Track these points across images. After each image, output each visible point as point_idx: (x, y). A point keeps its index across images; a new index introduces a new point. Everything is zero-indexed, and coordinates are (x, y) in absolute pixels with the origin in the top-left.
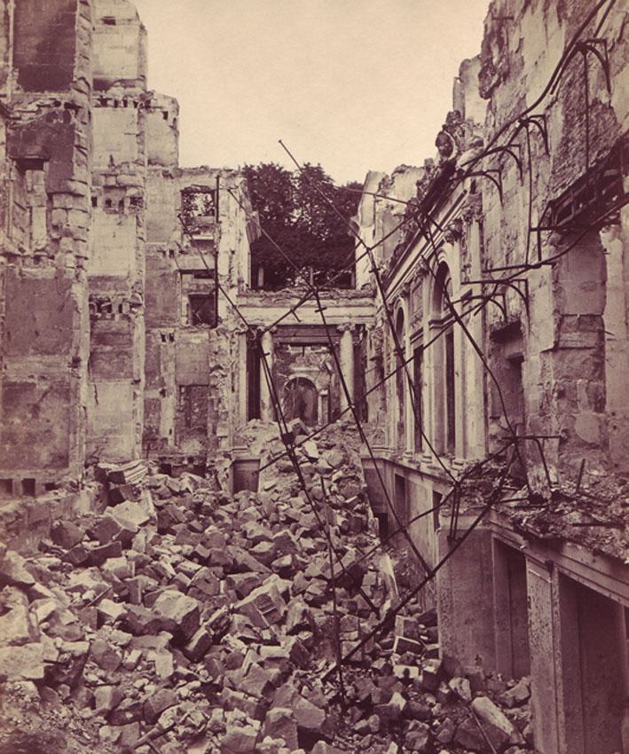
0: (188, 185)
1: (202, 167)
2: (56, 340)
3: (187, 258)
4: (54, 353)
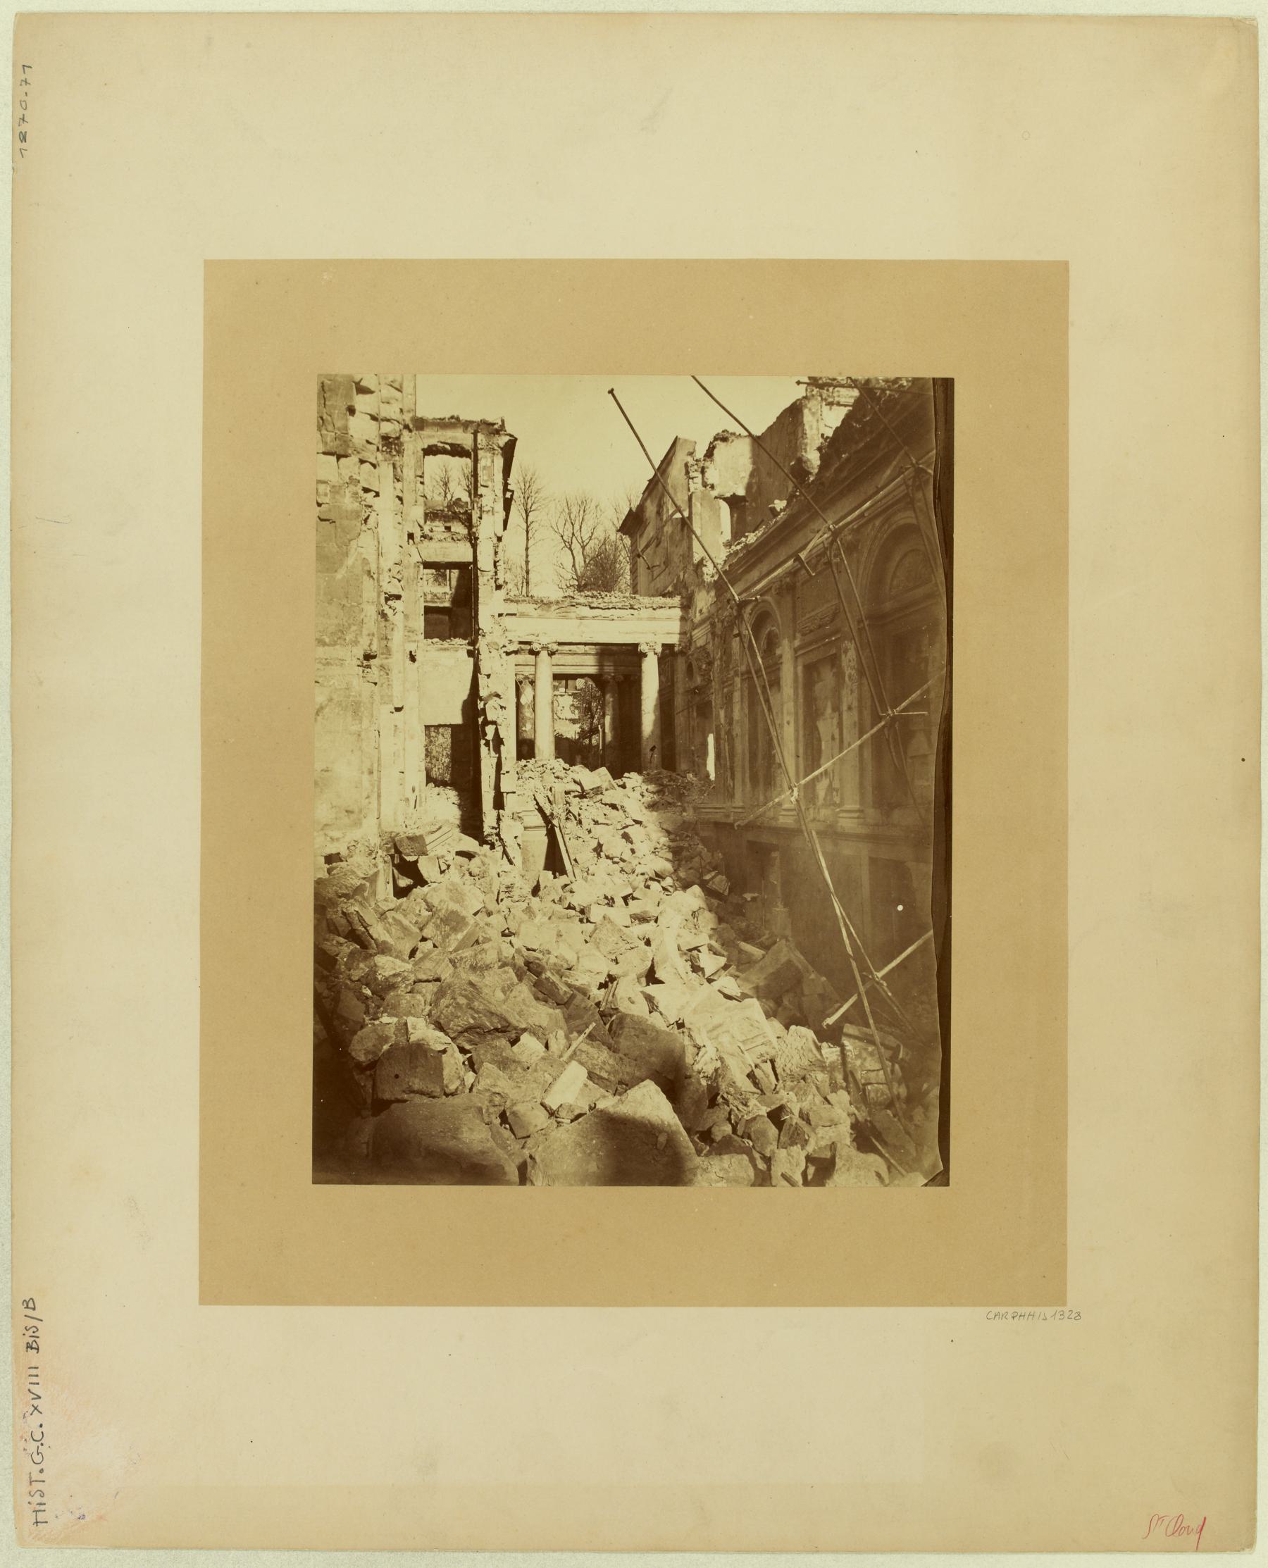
0: (433, 442)
1: (452, 417)
2: (336, 621)
3: (432, 544)
4: (334, 644)
